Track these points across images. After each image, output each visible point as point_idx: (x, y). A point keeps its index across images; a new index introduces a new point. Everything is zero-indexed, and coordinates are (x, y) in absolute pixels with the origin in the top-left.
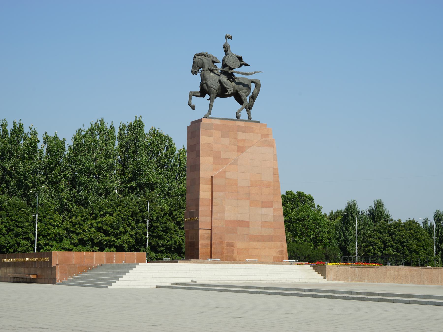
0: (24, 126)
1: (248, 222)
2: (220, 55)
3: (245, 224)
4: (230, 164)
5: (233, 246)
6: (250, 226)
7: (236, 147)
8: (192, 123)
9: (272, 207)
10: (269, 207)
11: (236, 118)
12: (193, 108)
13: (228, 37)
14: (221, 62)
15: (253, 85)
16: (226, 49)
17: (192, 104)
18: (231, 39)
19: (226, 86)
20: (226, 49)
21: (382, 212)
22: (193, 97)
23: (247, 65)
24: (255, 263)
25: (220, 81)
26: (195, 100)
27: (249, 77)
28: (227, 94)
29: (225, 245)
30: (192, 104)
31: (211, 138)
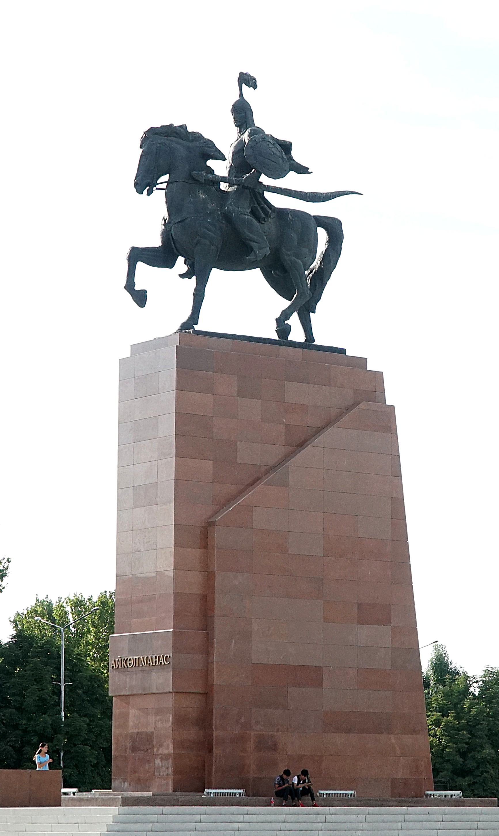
0: (278, 316)
1: (318, 669)
2: (225, 137)
3: (311, 676)
4: (266, 484)
5: (274, 747)
6: (325, 684)
7: (282, 428)
8: (135, 348)
9: (387, 621)
10: (378, 622)
11: (275, 337)
12: (140, 298)
13: (246, 80)
14: (229, 156)
15: (322, 235)
16: (242, 114)
17: (137, 288)
18: (255, 87)
19: (248, 234)
20: (242, 114)
21: (446, 665)
22: (141, 266)
23: (302, 170)
24: (345, 802)
25: (227, 218)
26: (146, 275)
27: (314, 209)
28: (252, 257)
29: (251, 745)
30: (137, 288)
31: (208, 399)
